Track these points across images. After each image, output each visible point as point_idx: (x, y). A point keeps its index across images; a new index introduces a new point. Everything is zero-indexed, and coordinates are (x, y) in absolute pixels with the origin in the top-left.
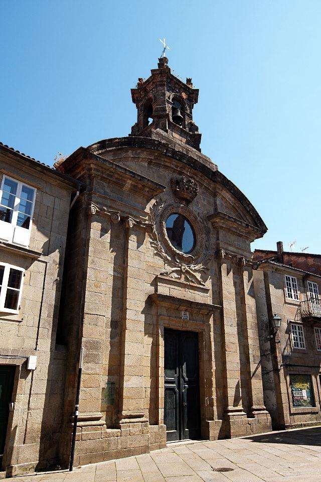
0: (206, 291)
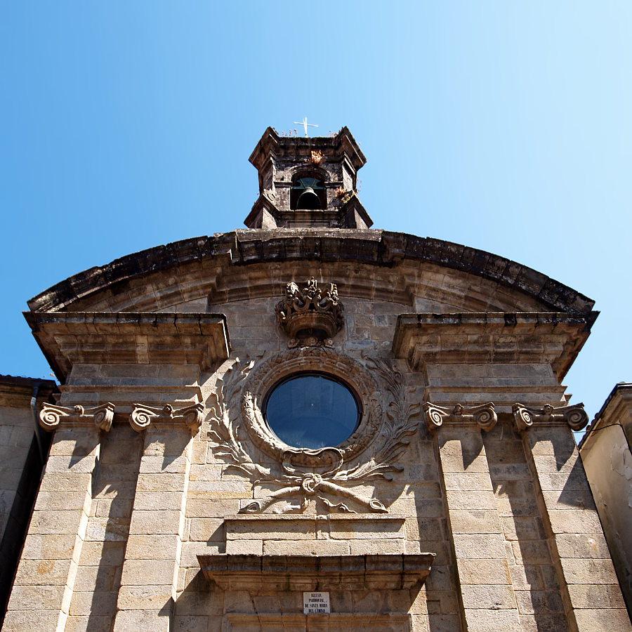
0: (395, 524)
